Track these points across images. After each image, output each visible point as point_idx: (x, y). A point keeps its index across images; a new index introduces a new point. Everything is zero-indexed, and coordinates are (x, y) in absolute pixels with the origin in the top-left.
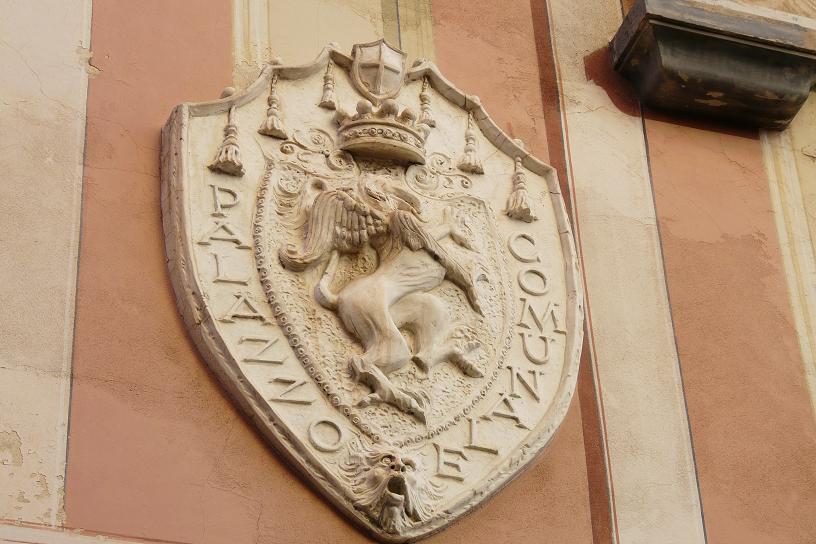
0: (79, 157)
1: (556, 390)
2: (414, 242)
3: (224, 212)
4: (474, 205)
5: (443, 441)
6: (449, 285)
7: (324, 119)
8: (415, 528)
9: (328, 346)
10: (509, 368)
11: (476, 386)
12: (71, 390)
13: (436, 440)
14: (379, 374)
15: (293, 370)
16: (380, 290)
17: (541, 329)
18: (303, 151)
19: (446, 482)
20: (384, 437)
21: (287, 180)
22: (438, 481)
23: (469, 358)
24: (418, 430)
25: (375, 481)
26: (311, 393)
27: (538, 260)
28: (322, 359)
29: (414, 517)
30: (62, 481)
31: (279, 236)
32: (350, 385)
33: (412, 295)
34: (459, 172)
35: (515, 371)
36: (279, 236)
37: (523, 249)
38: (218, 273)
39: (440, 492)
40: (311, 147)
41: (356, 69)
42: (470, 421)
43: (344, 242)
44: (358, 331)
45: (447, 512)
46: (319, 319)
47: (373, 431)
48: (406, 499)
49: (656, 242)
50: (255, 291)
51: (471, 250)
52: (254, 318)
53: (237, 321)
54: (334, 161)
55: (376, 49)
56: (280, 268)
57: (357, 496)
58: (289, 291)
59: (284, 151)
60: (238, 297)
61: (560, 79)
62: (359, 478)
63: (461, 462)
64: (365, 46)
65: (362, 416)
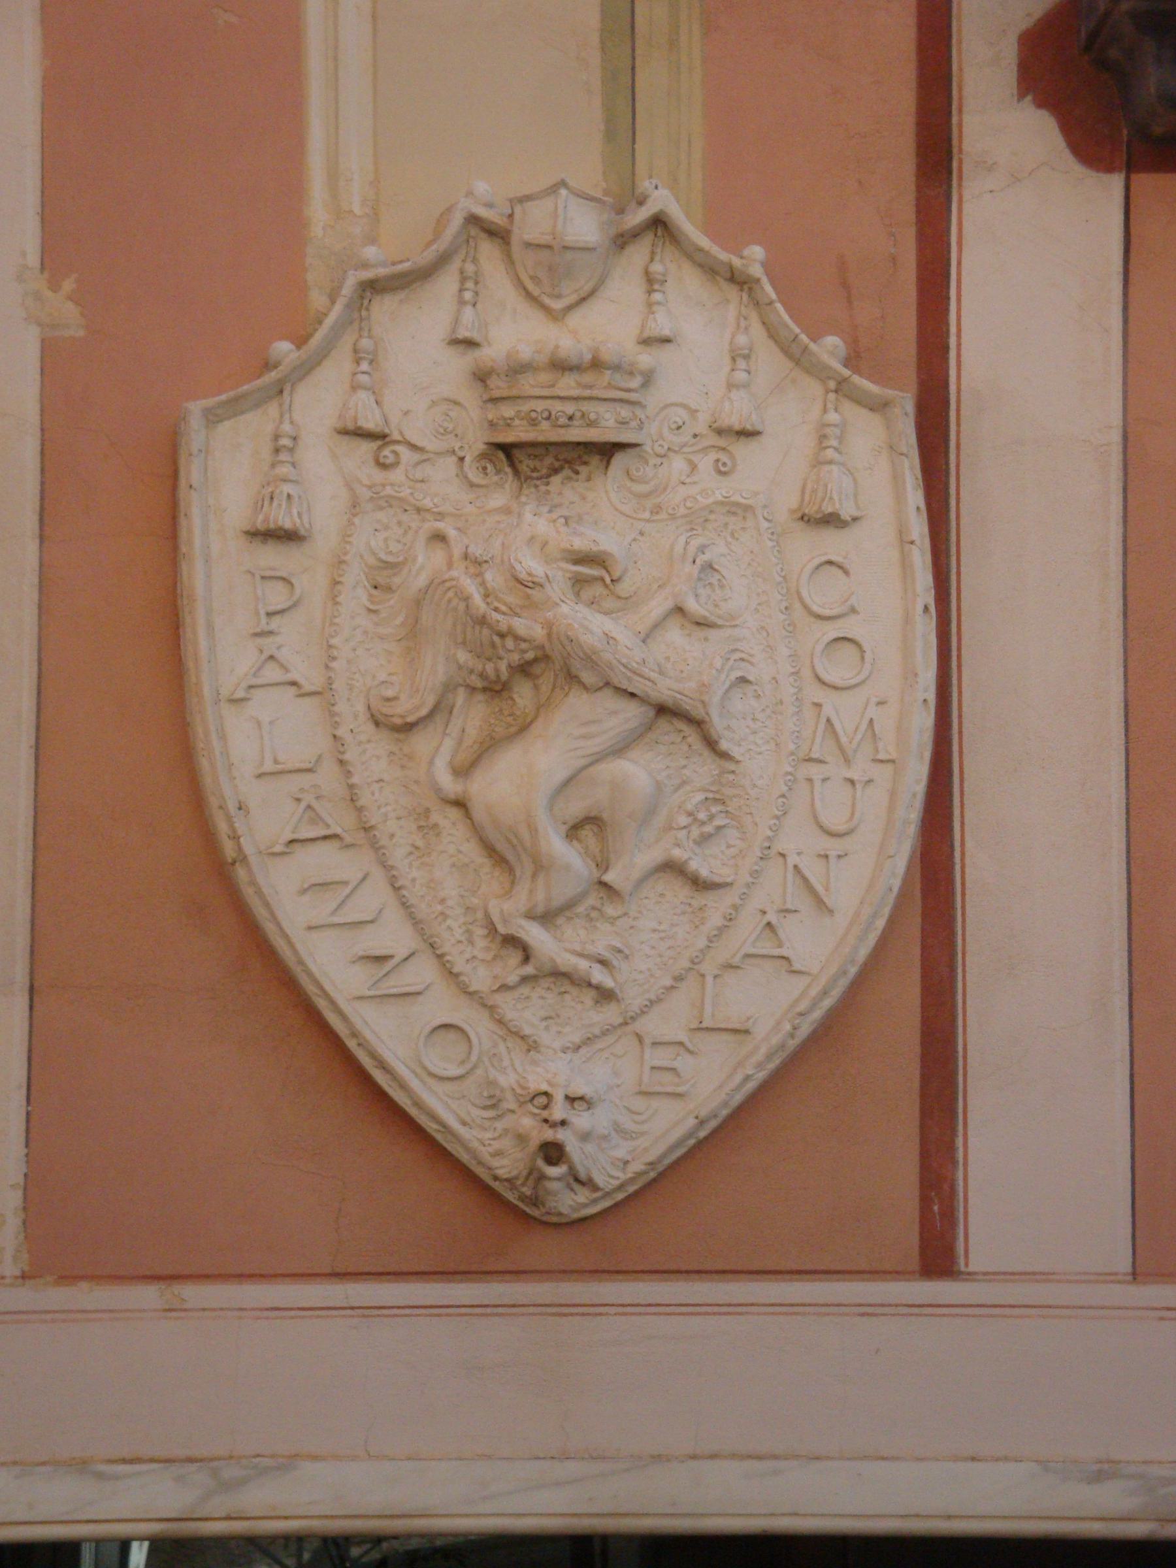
0: (29, 522)
1: (868, 873)
2: (587, 677)
3: (275, 622)
4: (734, 514)
5: (651, 1026)
6: (663, 724)
7: (455, 367)
8: (595, 1201)
9: (448, 872)
10: (783, 855)
11: (717, 906)
12: (31, 1017)
13: (638, 1026)
14: (534, 934)
15: (394, 936)
16: (526, 777)
17: (847, 761)
18: (417, 457)
19: (655, 1103)
20: (545, 1038)
21: (387, 528)
22: (639, 1104)
23: (700, 866)
24: (610, 1014)
25: (521, 1139)
26: (422, 972)
27: (853, 610)
28: (439, 908)
29: (588, 1183)
30: (20, 1193)
31: (373, 665)
32: (487, 949)
33: (591, 769)
34: (714, 440)
35: (792, 860)
36: (373, 665)
37: (825, 594)
38: (263, 740)
39: (643, 1122)
40: (431, 444)
41: (516, 247)
42: (703, 976)
43: (473, 677)
44: (502, 853)
45: (651, 1164)
46: (436, 825)
47: (527, 1031)
48: (572, 1168)
49: (1116, 486)
50: (328, 778)
51: (720, 627)
52: (325, 838)
53: (297, 846)
54: (474, 476)
55: (548, 203)
56: (371, 727)
57: (495, 1163)
58: (386, 777)
59: (383, 466)
60: (298, 800)
61: (960, 111)
62: (500, 1125)
63: (684, 1063)
64: (528, 198)
65: (507, 1004)
